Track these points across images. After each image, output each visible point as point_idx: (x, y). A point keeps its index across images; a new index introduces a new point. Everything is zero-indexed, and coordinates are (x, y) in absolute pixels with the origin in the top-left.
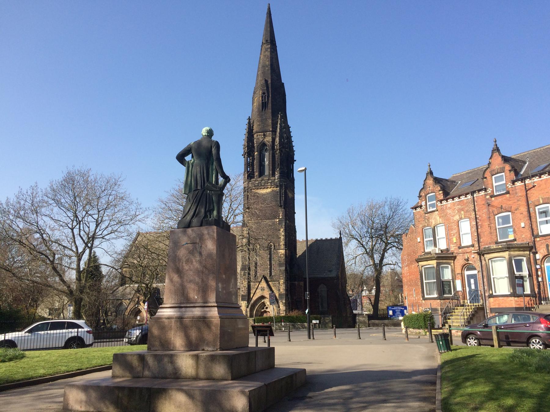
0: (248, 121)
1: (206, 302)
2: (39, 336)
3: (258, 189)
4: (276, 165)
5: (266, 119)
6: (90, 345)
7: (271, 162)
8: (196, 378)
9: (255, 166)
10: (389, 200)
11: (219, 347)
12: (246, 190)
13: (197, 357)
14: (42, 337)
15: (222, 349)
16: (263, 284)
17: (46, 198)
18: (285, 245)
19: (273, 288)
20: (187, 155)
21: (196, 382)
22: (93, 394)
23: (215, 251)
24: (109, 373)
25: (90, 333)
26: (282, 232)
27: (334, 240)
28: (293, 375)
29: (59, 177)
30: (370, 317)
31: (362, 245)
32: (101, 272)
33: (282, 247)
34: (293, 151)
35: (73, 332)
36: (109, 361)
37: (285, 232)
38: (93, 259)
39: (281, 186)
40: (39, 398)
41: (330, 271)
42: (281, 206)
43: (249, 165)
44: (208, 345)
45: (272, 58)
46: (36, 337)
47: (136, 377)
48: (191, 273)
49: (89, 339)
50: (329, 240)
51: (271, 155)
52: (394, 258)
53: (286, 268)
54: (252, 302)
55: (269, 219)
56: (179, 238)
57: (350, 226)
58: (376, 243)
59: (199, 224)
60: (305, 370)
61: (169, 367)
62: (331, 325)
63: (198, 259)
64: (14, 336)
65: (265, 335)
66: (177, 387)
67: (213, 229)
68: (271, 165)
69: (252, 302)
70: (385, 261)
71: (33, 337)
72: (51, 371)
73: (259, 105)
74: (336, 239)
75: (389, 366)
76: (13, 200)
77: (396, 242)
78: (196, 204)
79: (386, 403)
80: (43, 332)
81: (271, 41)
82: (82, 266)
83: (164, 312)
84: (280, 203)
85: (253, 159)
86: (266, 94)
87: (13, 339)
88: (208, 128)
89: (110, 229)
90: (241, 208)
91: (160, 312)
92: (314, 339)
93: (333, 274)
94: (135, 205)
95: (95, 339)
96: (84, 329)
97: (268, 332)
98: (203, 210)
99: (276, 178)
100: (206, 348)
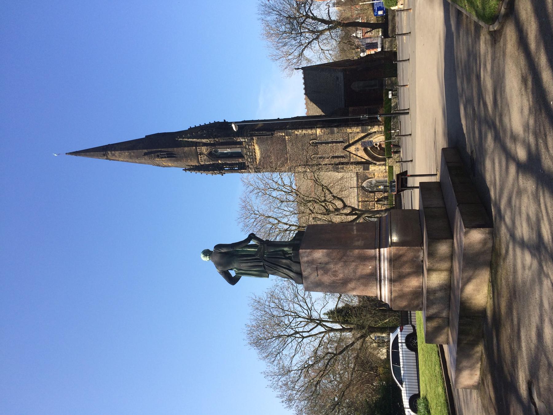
0: (187, 171)
1: (375, 257)
2: (406, 375)
3: (256, 159)
4: (231, 140)
5: (184, 153)
6: (414, 327)
7: (228, 146)
8: (451, 271)
9: (233, 162)
10: (260, 16)
11: (420, 248)
12: (257, 170)
13: (430, 270)
14: (406, 372)
15: (422, 244)
16: (352, 149)
17: (276, 362)
18: (311, 128)
19: (356, 139)
20: (230, 274)
21: (455, 273)
22: (465, 363)
23: (325, 251)
24: (445, 347)
25: (403, 329)
26: (299, 132)
27: (304, 76)
28: (448, 166)
29: (254, 352)
30: (385, 35)
31: (309, 43)
32: (343, 307)
33: (314, 131)
34: (215, 123)
35: (402, 348)
36: (433, 347)
37: (298, 129)
38: (331, 314)
39: (252, 136)
40: (467, 404)
41: (337, 78)
42: (272, 134)
43: (232, 169)
44: (418, 257)
45: (121, 149)
46: (406, 378)
47: (448, 322)
48: (346, 272)
49: (408, 329)
50: (305, 81)
51: (221, 147)
52: (321, 7)
53: (335, 127)
54: (370, 159)
55: (286, 146)
56: (312, 283)
57: (290, 57)
58: (307, 28)
59: (298, 265)
60: (443, 150)
61: (439, 294)
62: (394, 78)
63: (332, 266)
64: (406, 397)
65: (406, 179)
66: (460, 291)
67: (303, 253)
68: (230, 146)
69: (370, 159)
70: (326, 18)
71: (407, 380)
72: (440, 381)
73: (171, 160)
74: (304, 73)
75: (440, 48)
76: (278, 392)
77: (305, 6)
78: (278, 267)
79: (480, 77)
80: (402, 372)
81: (104, 151)
82: (337, 326)
83: (385, 296)
84: (269, 135)
85: (226, 164)
86: (159, 154)
87: (408, 398)
88: (202, 256)
89: (301, 303)
90: (276, 176)
91: (385, 300)
92: (409, 109)
93: (341, 75)
94: (278, 281)
95: (408, 324)
96: (400, 335)
97: (403, 177)
98: (284, 261)
99: (243, 140)
100: (421, 258)
